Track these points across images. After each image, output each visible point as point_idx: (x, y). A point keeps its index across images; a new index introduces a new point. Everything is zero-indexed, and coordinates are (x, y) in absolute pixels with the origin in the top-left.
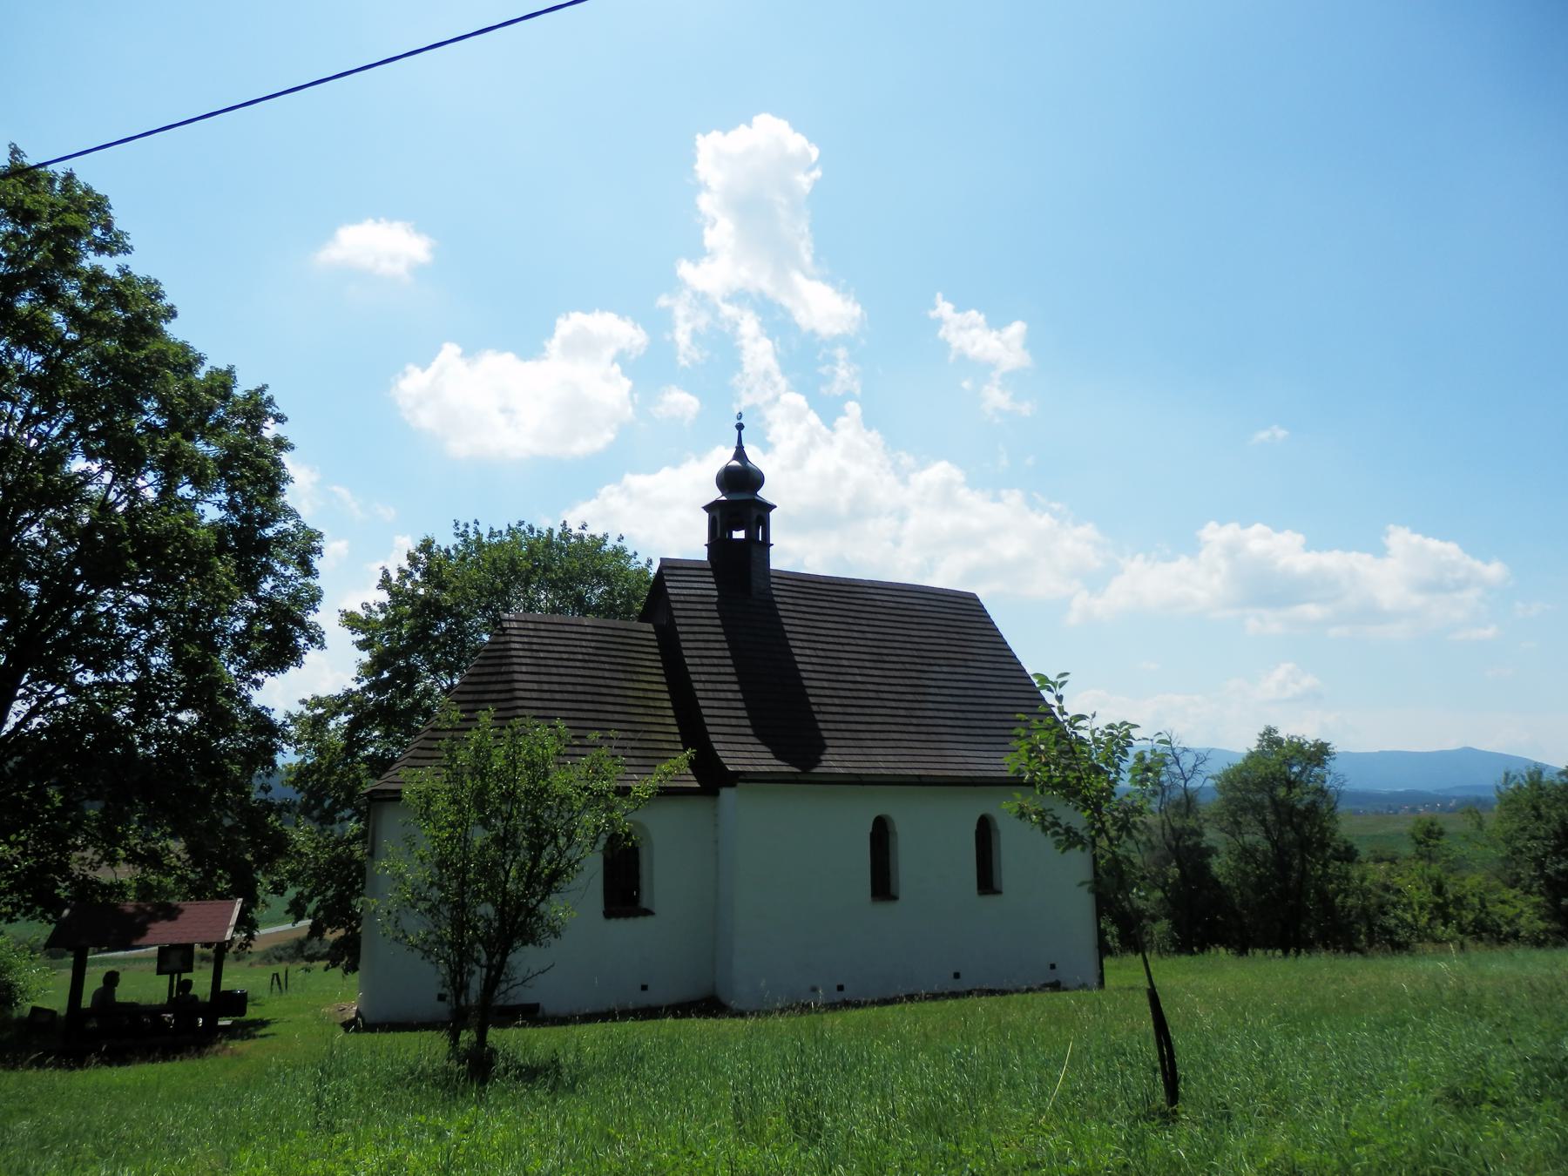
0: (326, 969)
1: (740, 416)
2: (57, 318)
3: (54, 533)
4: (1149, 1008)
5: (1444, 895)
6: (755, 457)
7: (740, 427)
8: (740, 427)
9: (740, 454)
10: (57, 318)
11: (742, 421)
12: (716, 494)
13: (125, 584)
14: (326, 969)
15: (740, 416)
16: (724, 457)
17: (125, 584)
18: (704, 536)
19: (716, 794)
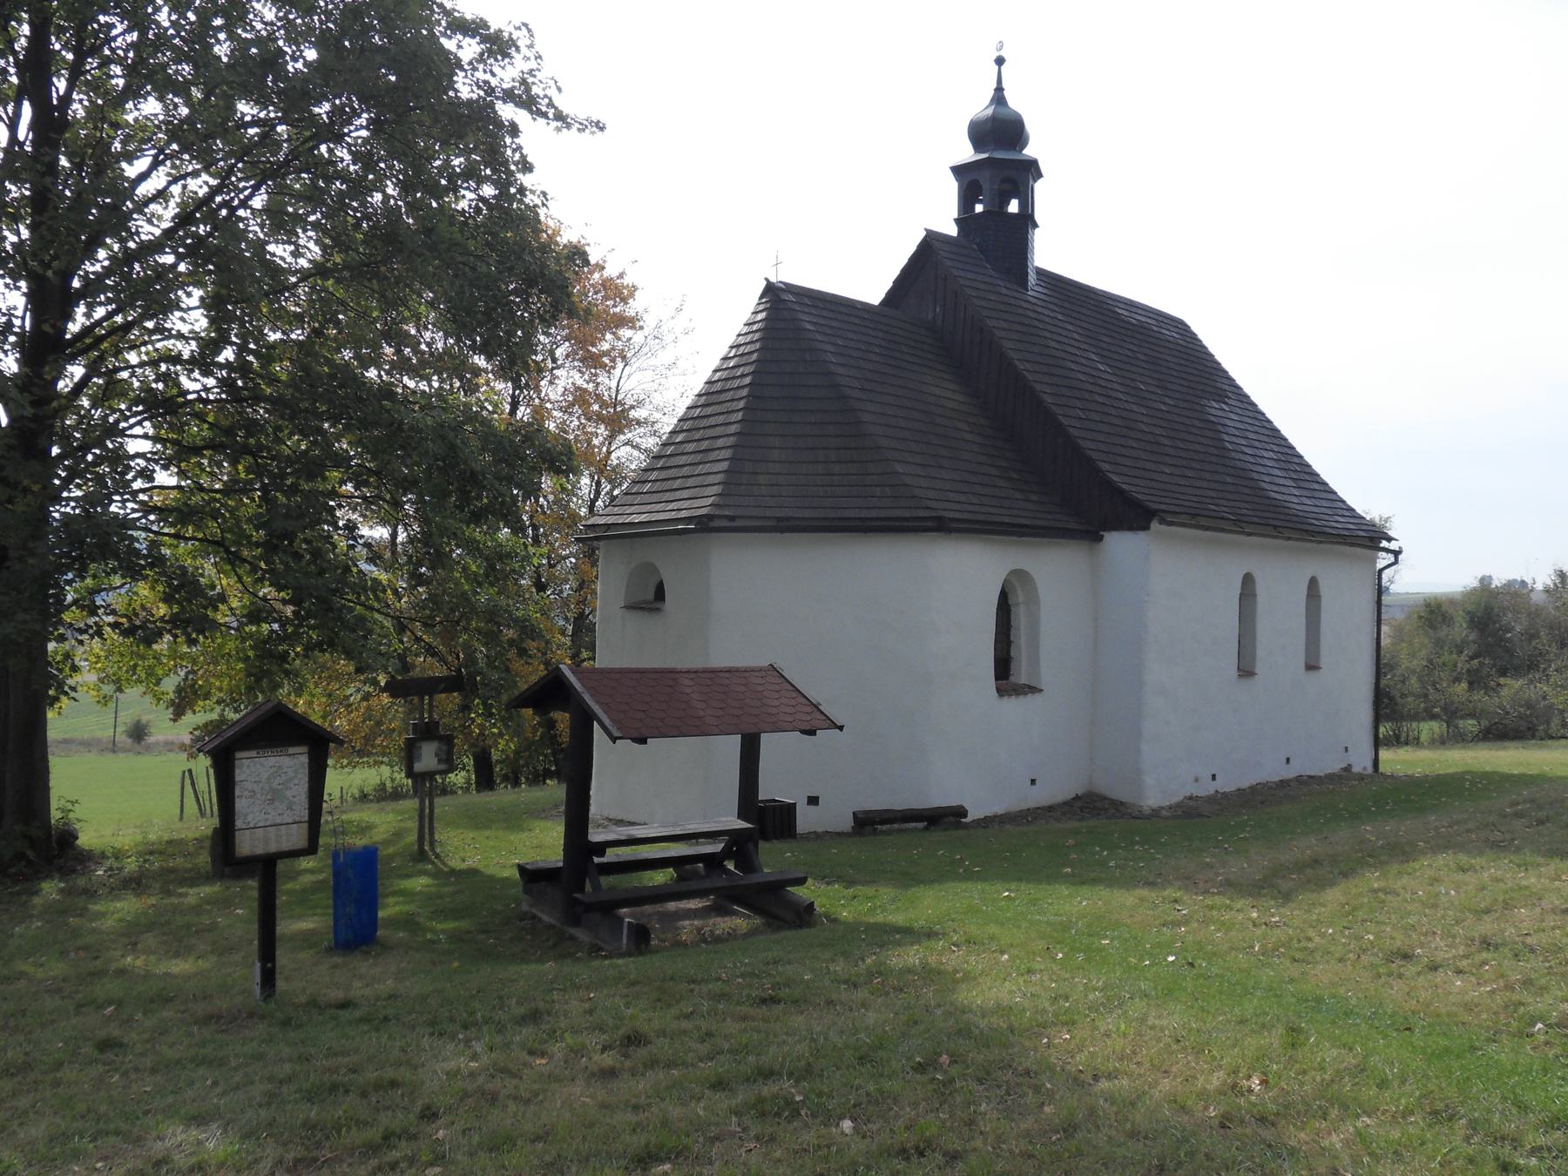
0: (640, 403)
1: (1001, 46)
2: (351, 213)
3: (131, 54)
4: (617, 666)
5: (226, 602)
6: (1015, 102)
7: (1000, 61)
8: (1000, 61)
9: (999, 97)
10: (351, 213)
11: (1003, 53)
12: (966, 153)
13: (180, 79)
14: (640, 403)
15: (1001, 46)
16: (979, 104)
17: (180, 79)
18: (953, 211)
19: (1100, 539)
